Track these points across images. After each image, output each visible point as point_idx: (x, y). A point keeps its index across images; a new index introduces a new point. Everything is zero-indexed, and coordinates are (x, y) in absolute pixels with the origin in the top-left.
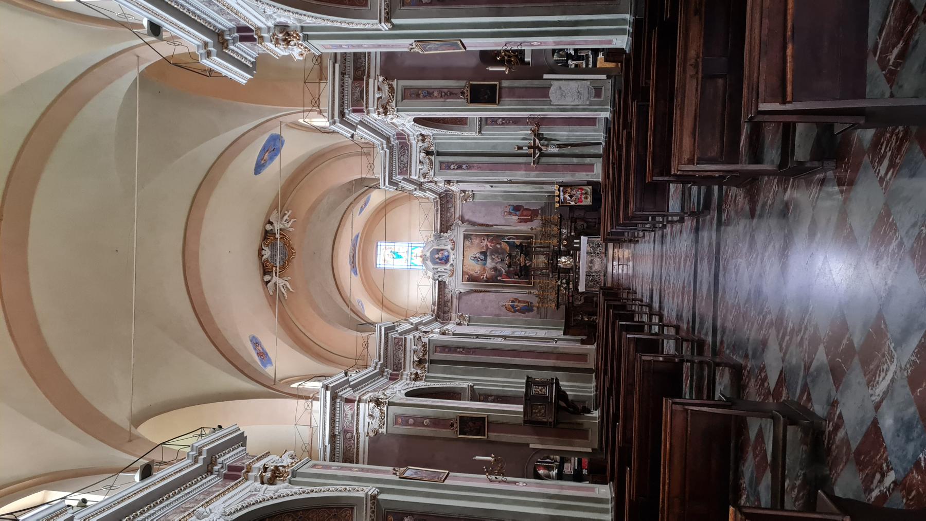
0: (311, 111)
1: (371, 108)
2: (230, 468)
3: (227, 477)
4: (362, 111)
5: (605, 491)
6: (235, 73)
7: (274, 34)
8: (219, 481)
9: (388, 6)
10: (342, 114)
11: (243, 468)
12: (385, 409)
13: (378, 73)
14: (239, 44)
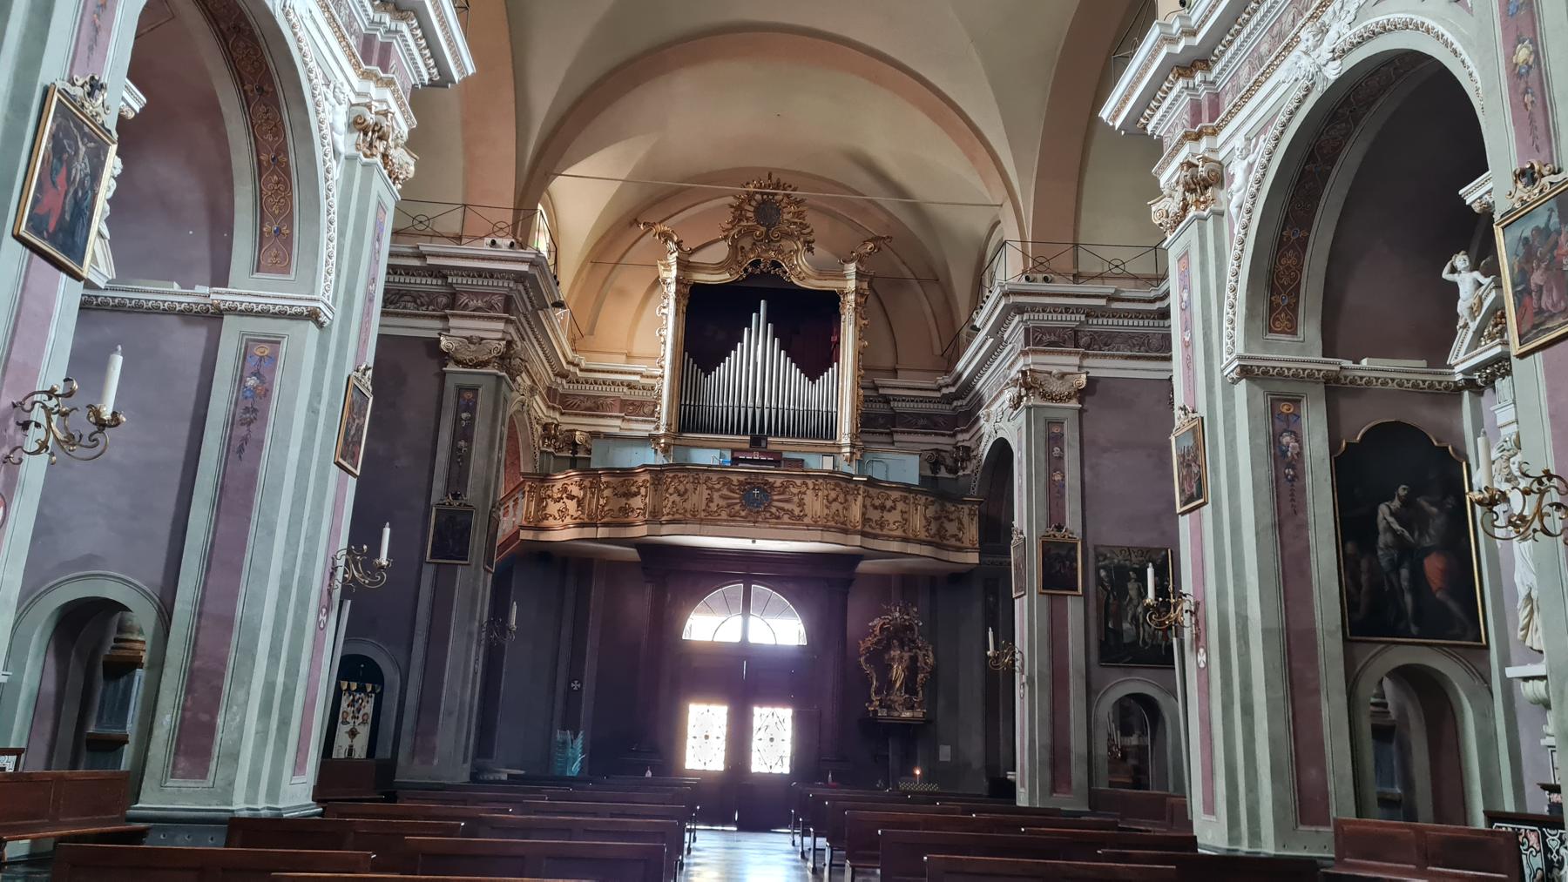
0: (1024, 254)
1: (1030, 359)
2: (386, 49)
3: (367, 42)
4: (1027, 344)
5: (1118, 124)
6: (1124, 100)
7: (1205, 160)
8: (362, 25)
9: (1266, 372)
10: (1020, 309)
11: (384, 66)
12: (489, 370)
13: (1093, 373)
14: (1186, 99)
